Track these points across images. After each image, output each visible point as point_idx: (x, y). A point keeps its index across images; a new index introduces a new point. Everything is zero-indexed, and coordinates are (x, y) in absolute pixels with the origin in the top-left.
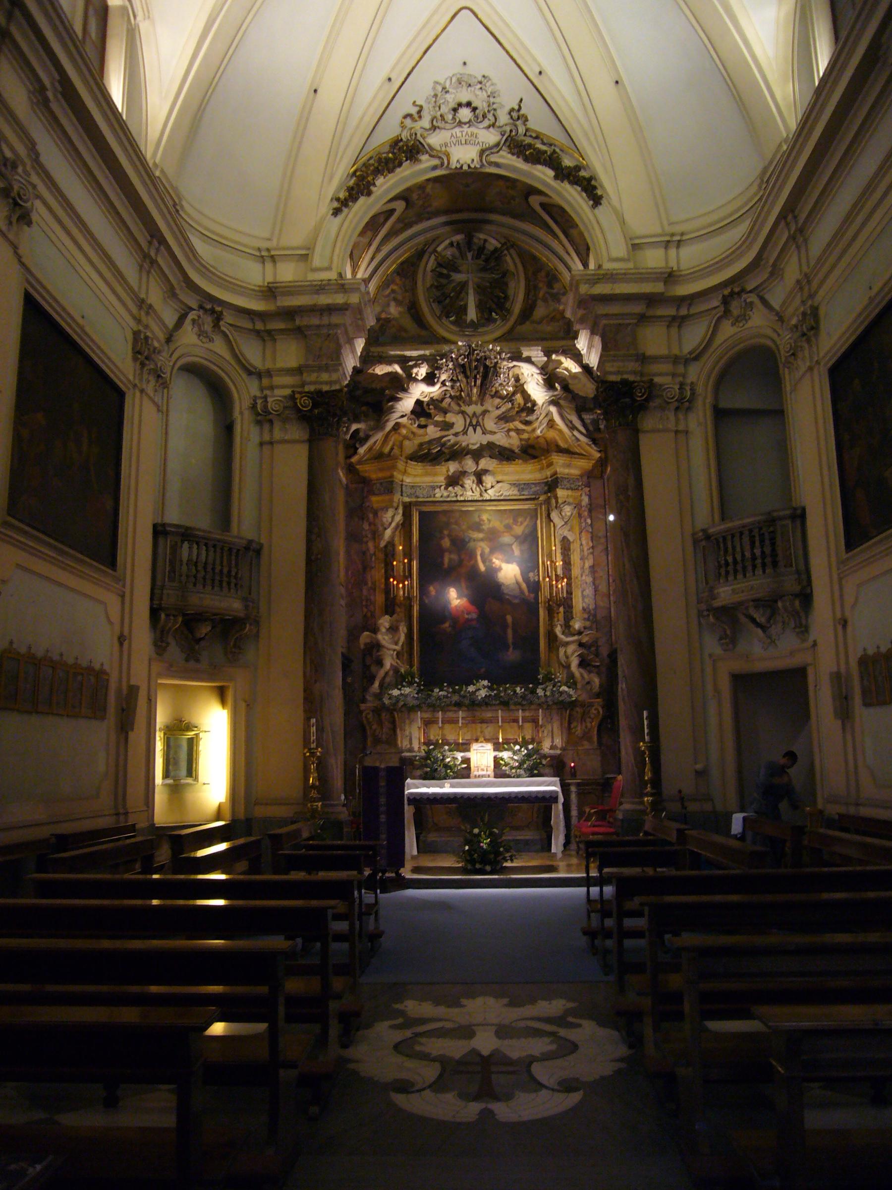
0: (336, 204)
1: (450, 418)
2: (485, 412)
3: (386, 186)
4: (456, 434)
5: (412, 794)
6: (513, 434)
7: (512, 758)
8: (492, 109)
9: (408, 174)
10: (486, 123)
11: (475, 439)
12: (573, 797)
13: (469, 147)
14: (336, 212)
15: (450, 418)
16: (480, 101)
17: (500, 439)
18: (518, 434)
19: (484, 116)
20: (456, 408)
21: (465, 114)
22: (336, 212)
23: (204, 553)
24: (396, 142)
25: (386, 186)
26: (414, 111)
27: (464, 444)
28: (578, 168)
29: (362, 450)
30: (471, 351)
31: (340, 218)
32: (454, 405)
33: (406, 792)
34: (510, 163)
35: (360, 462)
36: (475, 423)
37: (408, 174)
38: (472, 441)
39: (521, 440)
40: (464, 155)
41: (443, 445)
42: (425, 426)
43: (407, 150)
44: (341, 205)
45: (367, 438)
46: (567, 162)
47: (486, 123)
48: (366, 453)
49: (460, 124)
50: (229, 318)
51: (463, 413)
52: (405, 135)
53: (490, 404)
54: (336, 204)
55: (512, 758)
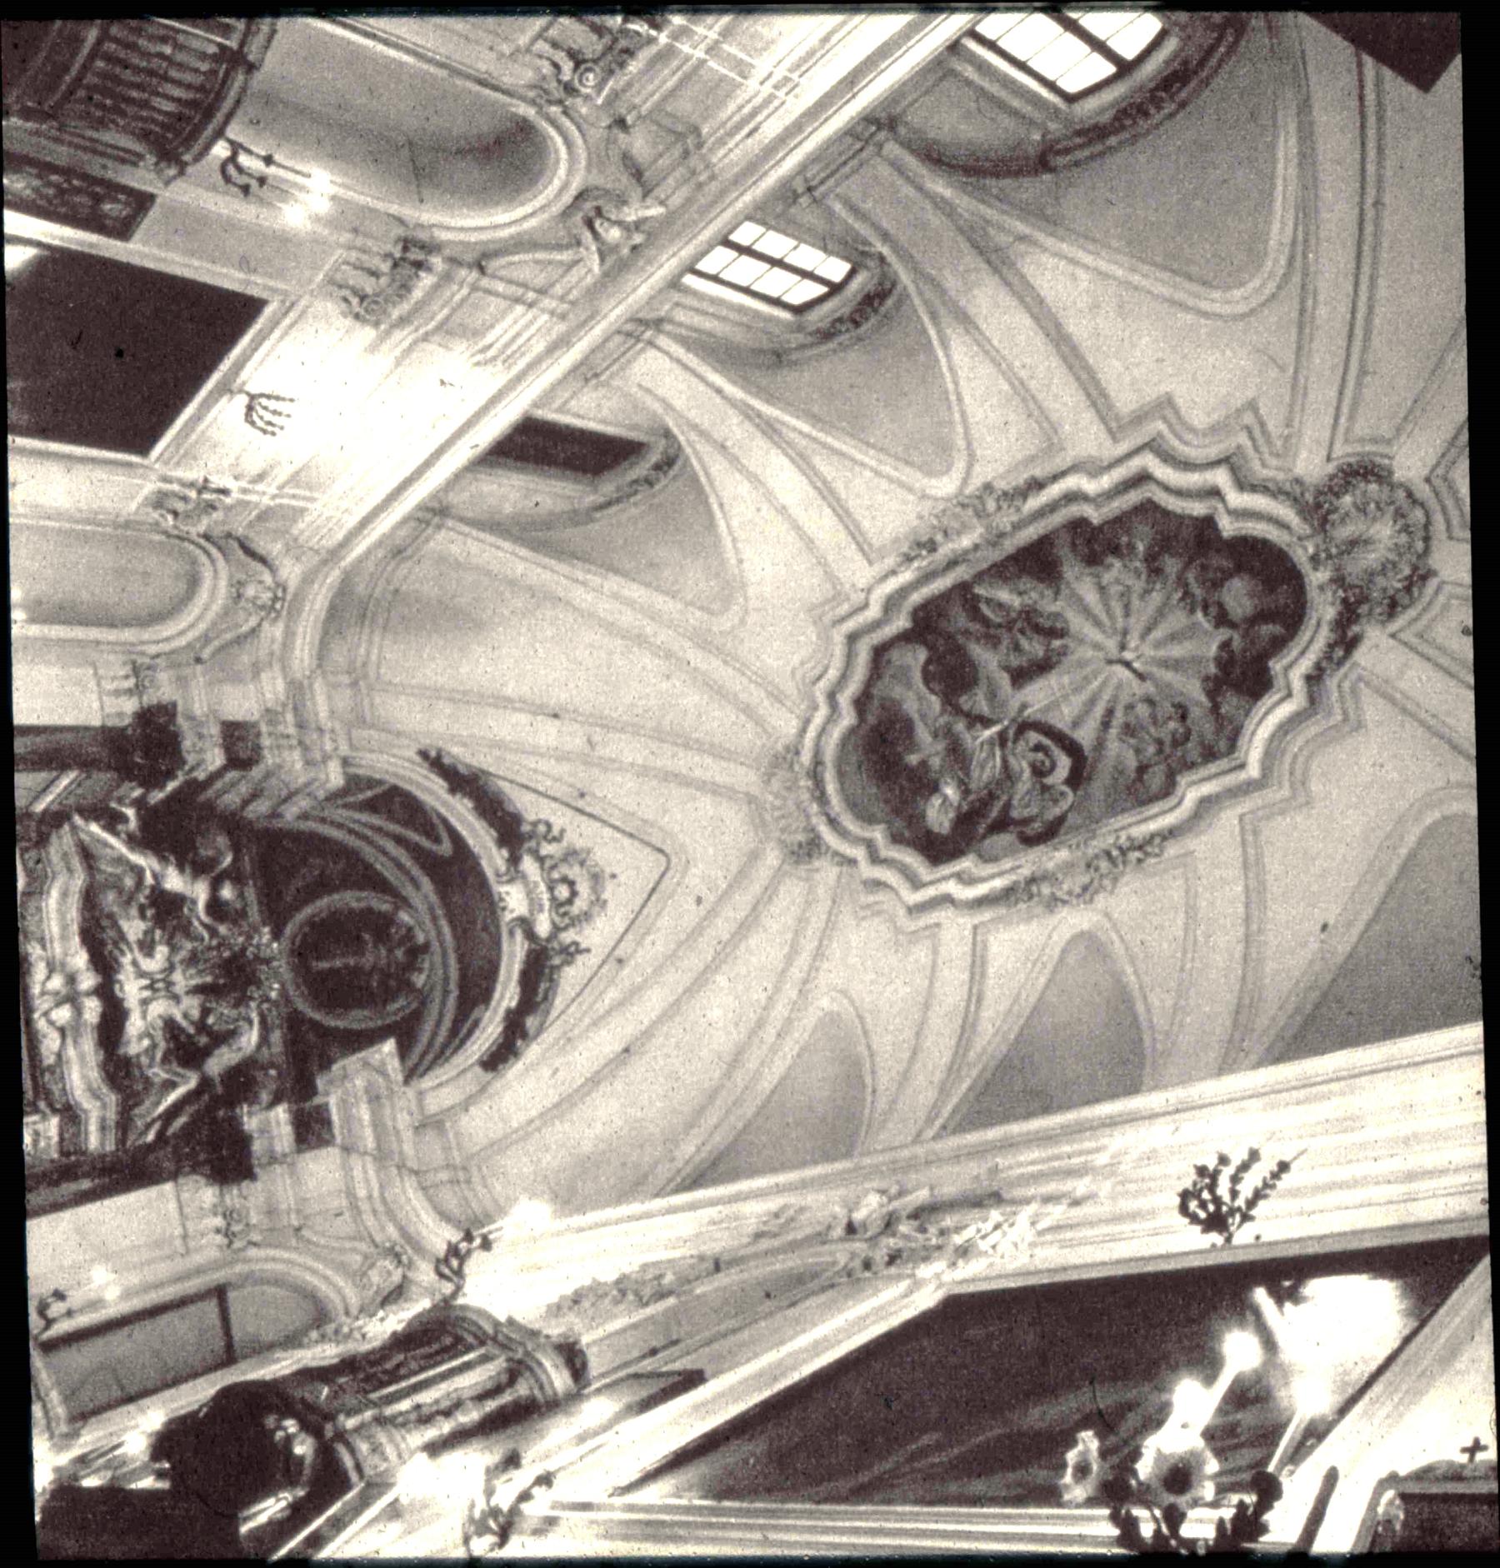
0: (433, 754)
1: (162, 951)
2: (176, 998)
3: (460, 813)
4: (135, 963)
5: (251, 1531)
6: (146, 1042)
7: (273, 641)
8: (575, 921)
9: (480, 837)
10: (557, 919)
11: (131, 989)
12: (432, 69)
13: (525, 903)
14: (424, 754)
15: (162, 951)
16: (580, 905)
17: (135, 1025)
18: (147, 1051)
19: (565, 914)
20: (177, 958)
21: (563, 892)
22: (424, 754)
23: (177, 92)
24: (516, 819)
25: (460, 813)
26: (555, 831)
27: (121, 977)
28: (524, 1035)
29: (94, 828)
30: (268, 961)
31: (418, 759)
32: (183, 954)
33: (48, 1463)
34: (513, 956)
35: (74, 828)
36: (159, 985)
37: (480, 837)
38: (127, 988)
39: (138, 1056)
40: (514, 900)
41: (116, 944)
42: (143, 916)
43: (511, 832)
44: (436, 763)
45: (116, 834)
46: (531, 1022)
47: (557, 919)
48: (91, 834)
49: (551, 889)
50: (453, 498)
51: (171, 968)
52: (526, 828)
53: (192, 1005)
54: (433, 754)
55: (273, 641)
